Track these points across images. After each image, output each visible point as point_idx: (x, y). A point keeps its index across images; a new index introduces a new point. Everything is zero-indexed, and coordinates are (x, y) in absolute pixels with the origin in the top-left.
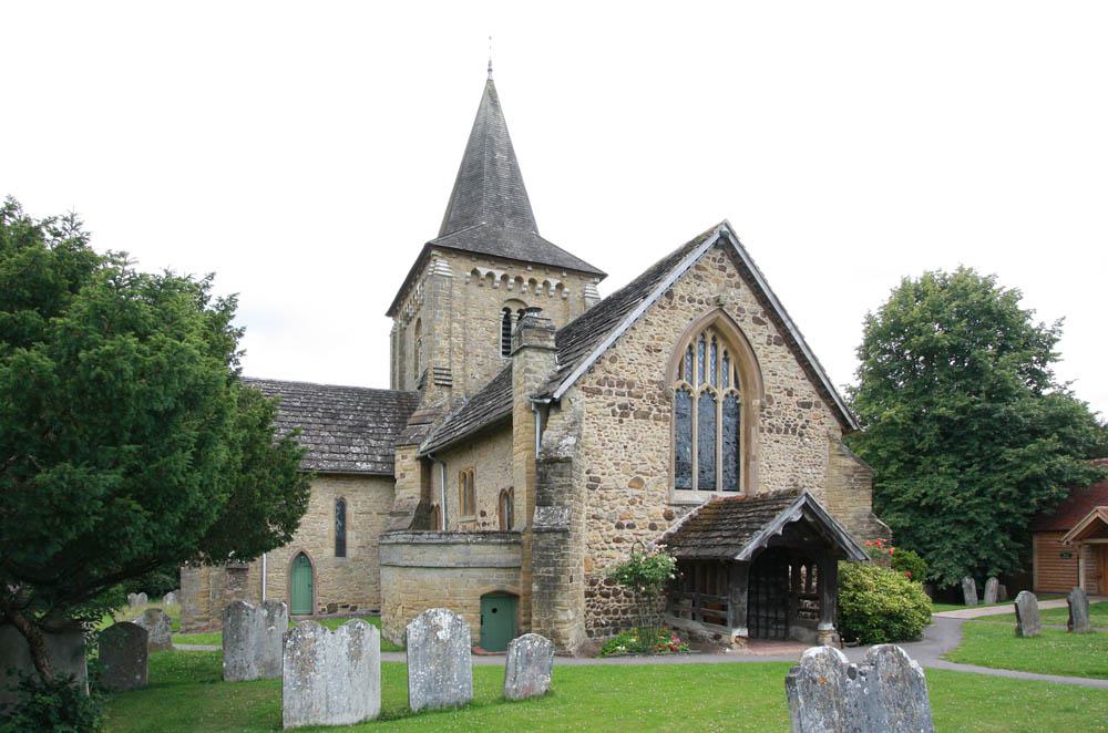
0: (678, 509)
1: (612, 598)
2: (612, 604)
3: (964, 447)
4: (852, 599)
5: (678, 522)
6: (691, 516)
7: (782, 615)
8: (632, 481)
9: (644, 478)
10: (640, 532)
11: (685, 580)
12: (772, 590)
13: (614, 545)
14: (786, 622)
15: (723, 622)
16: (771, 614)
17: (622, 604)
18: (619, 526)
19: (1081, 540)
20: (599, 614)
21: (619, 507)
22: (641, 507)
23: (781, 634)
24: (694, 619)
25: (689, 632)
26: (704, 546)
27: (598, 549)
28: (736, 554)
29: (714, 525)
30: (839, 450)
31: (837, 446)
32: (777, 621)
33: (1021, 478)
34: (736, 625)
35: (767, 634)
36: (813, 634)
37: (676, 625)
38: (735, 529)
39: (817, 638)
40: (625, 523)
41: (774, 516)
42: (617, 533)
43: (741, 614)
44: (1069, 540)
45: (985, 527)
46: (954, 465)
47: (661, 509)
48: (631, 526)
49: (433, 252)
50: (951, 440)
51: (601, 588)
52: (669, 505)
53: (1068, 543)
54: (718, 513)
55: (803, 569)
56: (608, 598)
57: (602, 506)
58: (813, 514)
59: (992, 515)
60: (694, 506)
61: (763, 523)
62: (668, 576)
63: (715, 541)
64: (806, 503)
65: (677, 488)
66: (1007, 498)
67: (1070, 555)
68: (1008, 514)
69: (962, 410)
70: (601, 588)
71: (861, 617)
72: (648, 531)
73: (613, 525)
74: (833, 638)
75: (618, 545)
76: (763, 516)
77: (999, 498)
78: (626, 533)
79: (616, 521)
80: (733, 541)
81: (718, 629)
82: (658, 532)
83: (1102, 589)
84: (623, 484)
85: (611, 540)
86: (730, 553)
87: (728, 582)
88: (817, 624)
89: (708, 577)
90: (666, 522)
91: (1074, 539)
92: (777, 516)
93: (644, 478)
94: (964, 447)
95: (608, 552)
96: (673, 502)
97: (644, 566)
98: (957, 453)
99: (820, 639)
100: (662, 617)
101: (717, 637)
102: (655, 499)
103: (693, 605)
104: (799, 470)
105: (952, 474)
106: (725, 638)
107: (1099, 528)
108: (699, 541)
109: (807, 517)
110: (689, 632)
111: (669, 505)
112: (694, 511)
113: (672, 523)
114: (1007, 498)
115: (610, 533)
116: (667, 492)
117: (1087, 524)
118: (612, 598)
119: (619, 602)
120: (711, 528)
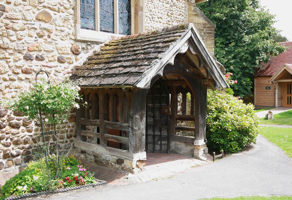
0: (84, 45)
1: (22, 128)
2: (23, 134)
3: (227, 34)
4: (216, 119)
5: (83, 57)
6: (94, 52)
7: (165, 133)
8: (39, 14)
9: (52, 13)
10: (49, 64)
11: (90, 108)
12: (157, 114)
13: (23, 76)
14: (168, 139)
15: (121, 146)
16: (157, 133)
17: (33, 133)
18: (28, 58)
19: (276, 80)
20: (7, 146)
21: (27, 39)
22: (49, 40)
23: (164, 148)
24: (98, 143)
25: (95, 156)
26: (106, 76)
27: (5, 80)
28: (138, 82)
29: (115, 57)
30: (194, 11)
31: (193, 8)
32: (161, 138)
33: (252, 50)
34: (136, 150)
35: (154, 148)
36: (189, 148)
37: (83, 148)
38: (133, 60)
39: (192, 151)
40: (34, 54)
41: (168, 46)
42: (26, 65)
43: (140, 140)
44: (272, 80)
45: (237, 74)
46: (222, 43)
47: (67, 45)
48: (40, 59)
49: (146, 159)
50: (221, 30)
51: (10, 119)
52: (76, 40)
53: (272, 82)
54: (117, 49)
55: (180, 97)
56: (19, 128)
57: (8, 36)
58: (196, 49)
59: (239, 68)
60: (97, 43)
61: (160, 52)
62: (71, 105)
63: (117, 71)
64: (191, 37)
65: (82, 28)
66: (246, 60)
67: (270, 88)
68: (246, 68)
69: (226, 15)
70: (10, 119)
71: (223, 132)
72: (56, 63)
73: (21, 56)
74: (204, 151)
75: (28, 76)
76: (158, 47)
77: (243, 60)
78: (35, 65)
79: (25, 52)
80: (133, 70)
81: (121, 153)
82: (66, 65)
83: (283, 104)
84: (31, 16)
85: (19, 71)
86: (132, 80)
87: (129, 108)
88: (193, 140)
89: (110, 105)
90: (73, 57)
91: (274, 80)
92: (171, 47)
93: (52, 13)
94: (227, 34)
95: (17, 83)
96: (78, 38)
97: (46, 96)
98: (223, 37)
99: (195, 152)
100: (72, 141)
101: (120, 161)
102: (63, 34)
103: (98, 131)
104: (170, 23)
105: (222, 47)
106: (127, 163)
107: (286, 74)
108: (102, 72)
109: (191, 49)
110: (95, 156)
111: (76, 40)
112: (97, 48)
113: (78, 57)
114: (246, 60)
115: (18, 64)
116: (73, 29)
117: (280, 73)
118: (22, 128)
119: (30, 131)
120: (112, 60)
